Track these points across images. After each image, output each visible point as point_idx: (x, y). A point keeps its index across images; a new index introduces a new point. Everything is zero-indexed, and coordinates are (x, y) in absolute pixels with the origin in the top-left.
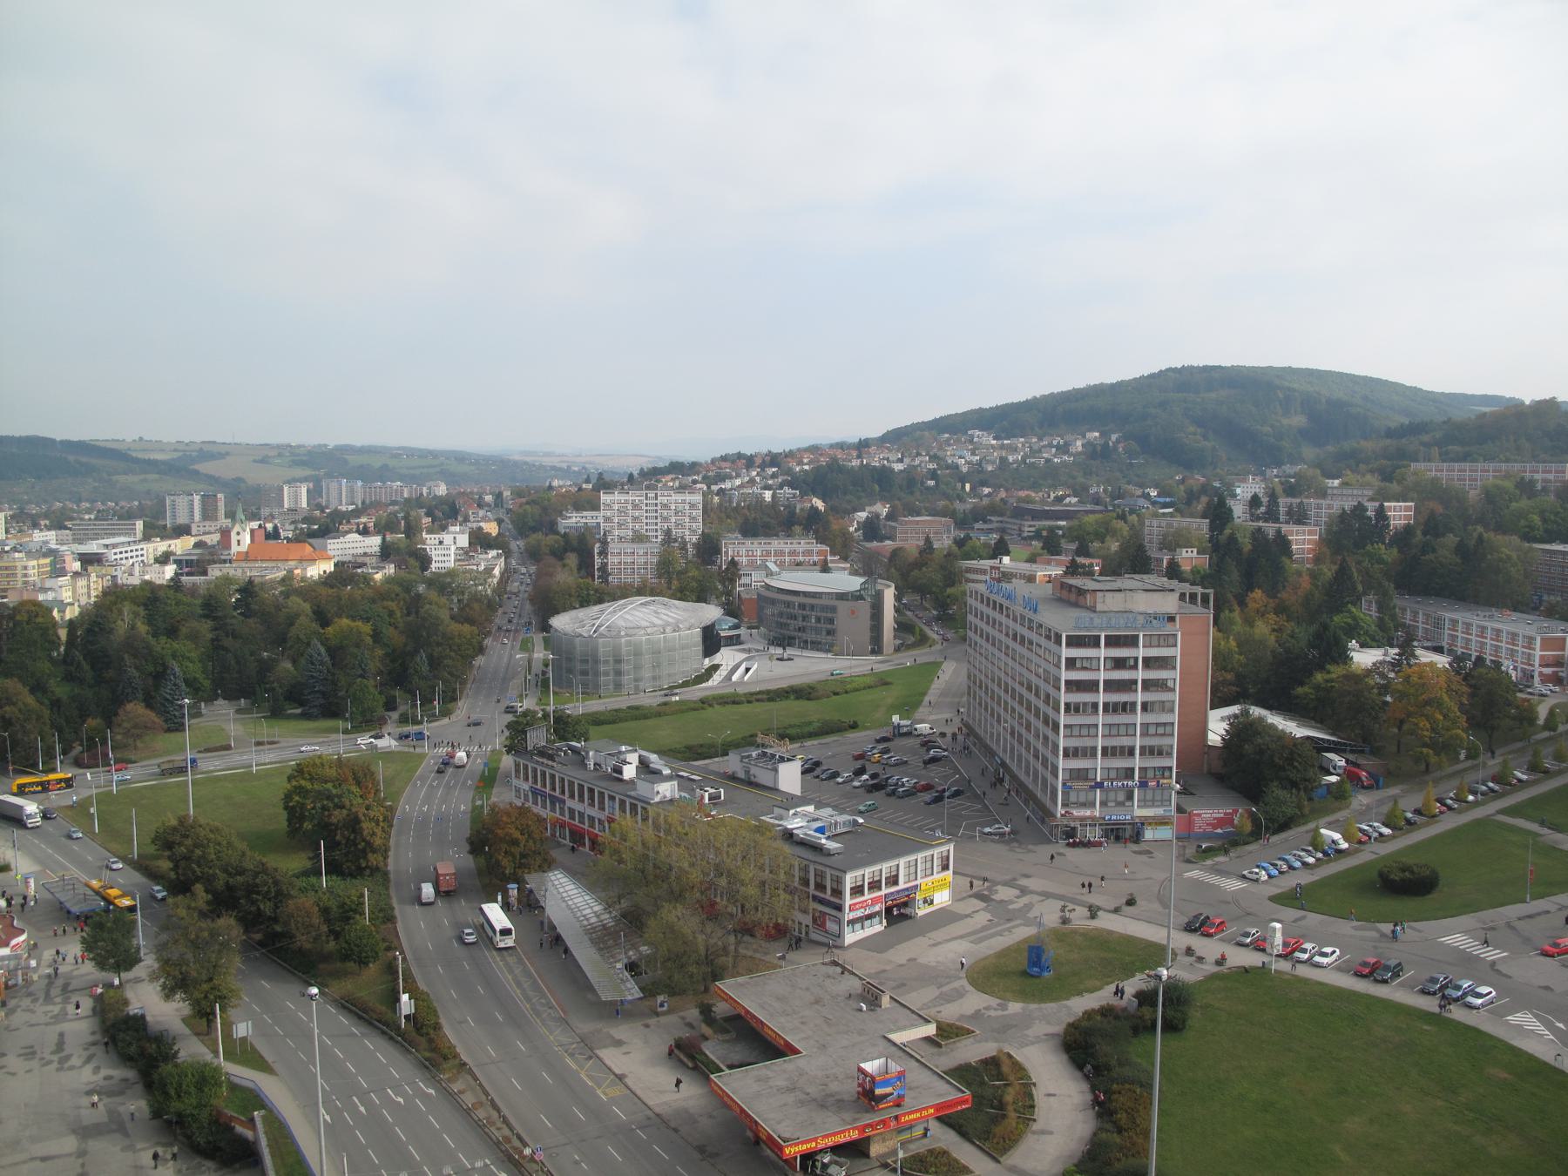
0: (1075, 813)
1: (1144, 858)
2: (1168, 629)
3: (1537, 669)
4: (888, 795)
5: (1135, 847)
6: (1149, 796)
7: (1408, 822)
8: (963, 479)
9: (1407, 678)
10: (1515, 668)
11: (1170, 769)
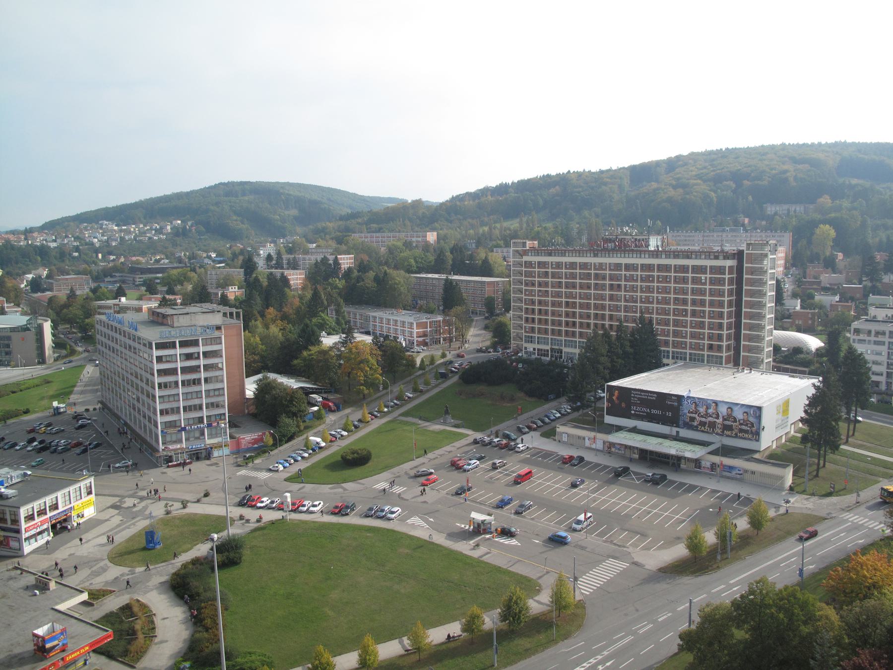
0: (171, 447)
1: (214, 467)
2: (217, 334)
3: (416, 339)
4: (52, 453)
5: (208, 462)
6: (214, 432)
7: (356, 427)
8: (97, 251)
9: (350, 350)
10: (405, 340)
11: (224, 414)
